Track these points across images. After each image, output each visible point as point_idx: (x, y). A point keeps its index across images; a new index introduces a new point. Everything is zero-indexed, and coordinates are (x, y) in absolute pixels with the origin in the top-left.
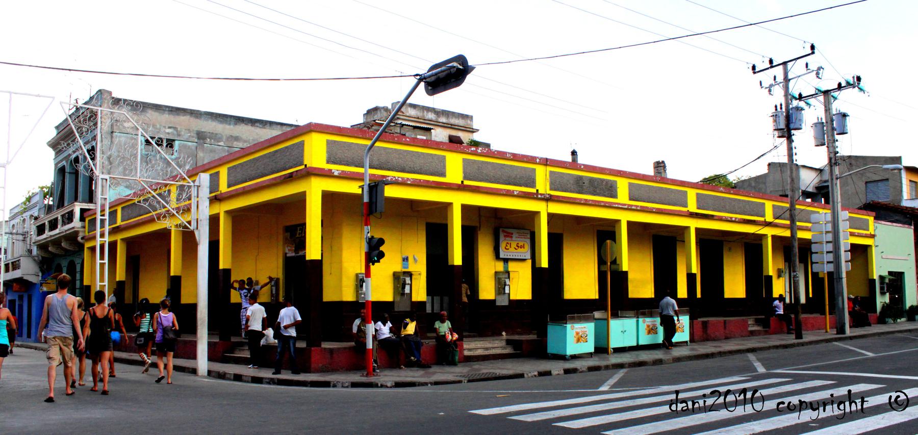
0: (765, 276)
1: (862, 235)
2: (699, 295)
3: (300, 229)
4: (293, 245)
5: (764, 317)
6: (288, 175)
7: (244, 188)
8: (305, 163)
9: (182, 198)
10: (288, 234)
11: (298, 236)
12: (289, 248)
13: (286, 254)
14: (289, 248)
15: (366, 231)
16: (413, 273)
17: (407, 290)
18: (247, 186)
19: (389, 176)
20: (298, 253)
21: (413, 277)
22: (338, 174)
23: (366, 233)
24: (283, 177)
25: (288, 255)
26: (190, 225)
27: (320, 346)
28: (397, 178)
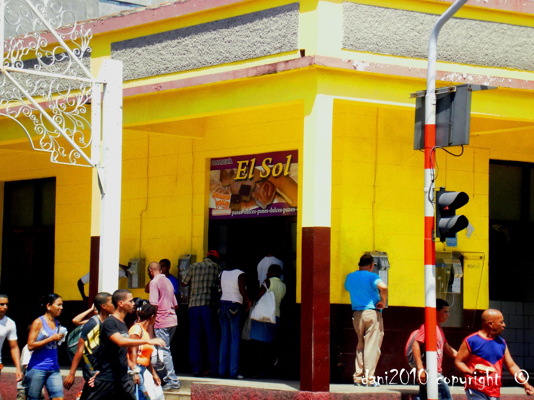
0: (305, 230)
1: (330, 66)
2: (299, 300)
3: (244, 165)
4: (227, 193)
5: (275, 365)
6: (267, 68)
7: (158, 87)
8: (300, 47)
9: (76, 103)
10: (217, 173)
11: (238, 177)
12: (218, 200)
13: (211, 210)
14: (218, 200)
15: (429, 179)
16: (465, 254)
17: (456, 289)
18: (165, 83)
19: (451, 73)
20: (239, 210)
21: (466, 263)
22: (365, 69)
23: (429, 182)
24: (254, 72)
25: (214, 213)
26: (89, 156)
27: (327, 389)
28: (465, 76)
